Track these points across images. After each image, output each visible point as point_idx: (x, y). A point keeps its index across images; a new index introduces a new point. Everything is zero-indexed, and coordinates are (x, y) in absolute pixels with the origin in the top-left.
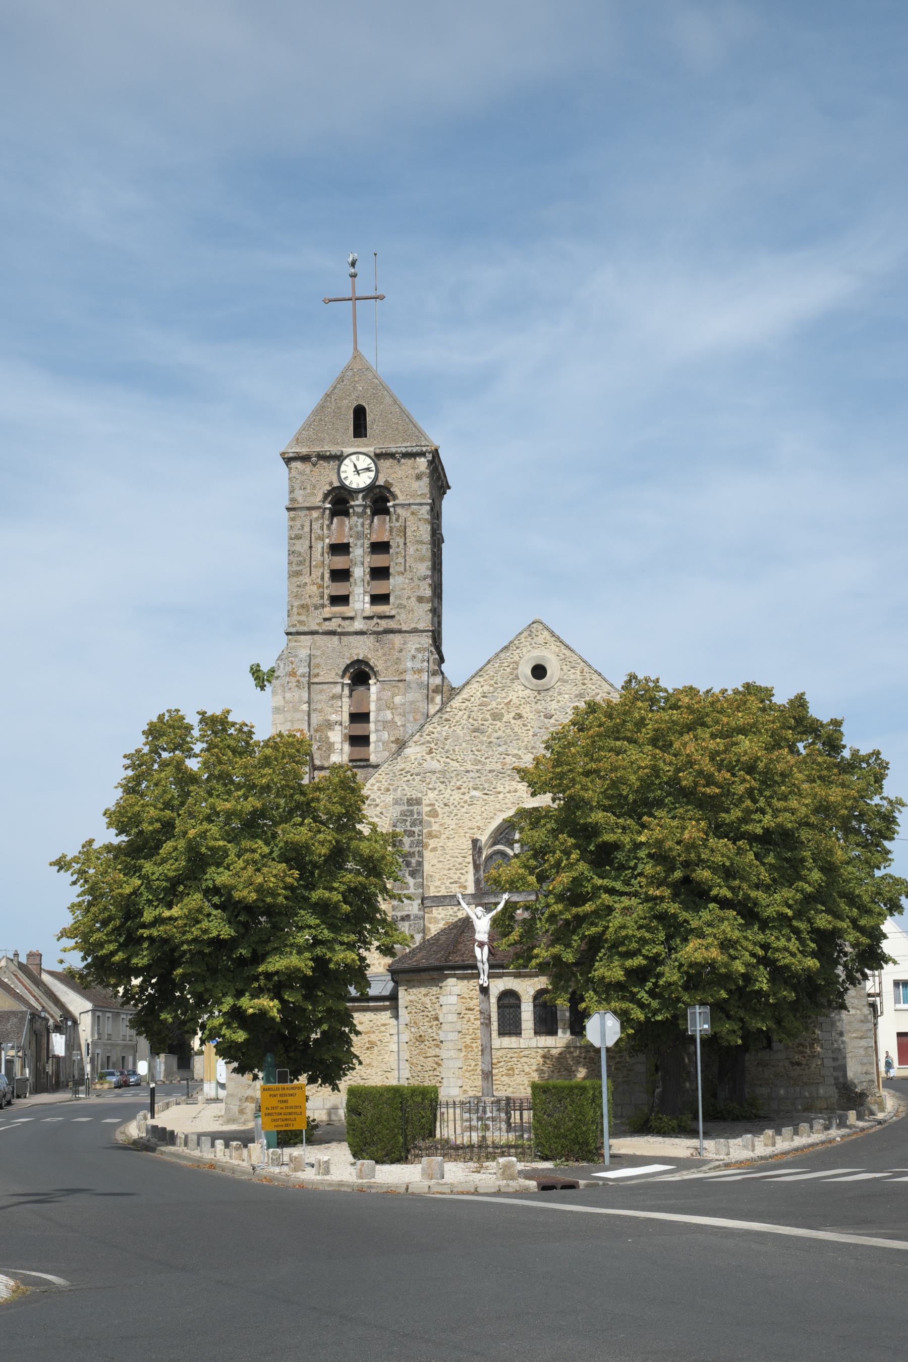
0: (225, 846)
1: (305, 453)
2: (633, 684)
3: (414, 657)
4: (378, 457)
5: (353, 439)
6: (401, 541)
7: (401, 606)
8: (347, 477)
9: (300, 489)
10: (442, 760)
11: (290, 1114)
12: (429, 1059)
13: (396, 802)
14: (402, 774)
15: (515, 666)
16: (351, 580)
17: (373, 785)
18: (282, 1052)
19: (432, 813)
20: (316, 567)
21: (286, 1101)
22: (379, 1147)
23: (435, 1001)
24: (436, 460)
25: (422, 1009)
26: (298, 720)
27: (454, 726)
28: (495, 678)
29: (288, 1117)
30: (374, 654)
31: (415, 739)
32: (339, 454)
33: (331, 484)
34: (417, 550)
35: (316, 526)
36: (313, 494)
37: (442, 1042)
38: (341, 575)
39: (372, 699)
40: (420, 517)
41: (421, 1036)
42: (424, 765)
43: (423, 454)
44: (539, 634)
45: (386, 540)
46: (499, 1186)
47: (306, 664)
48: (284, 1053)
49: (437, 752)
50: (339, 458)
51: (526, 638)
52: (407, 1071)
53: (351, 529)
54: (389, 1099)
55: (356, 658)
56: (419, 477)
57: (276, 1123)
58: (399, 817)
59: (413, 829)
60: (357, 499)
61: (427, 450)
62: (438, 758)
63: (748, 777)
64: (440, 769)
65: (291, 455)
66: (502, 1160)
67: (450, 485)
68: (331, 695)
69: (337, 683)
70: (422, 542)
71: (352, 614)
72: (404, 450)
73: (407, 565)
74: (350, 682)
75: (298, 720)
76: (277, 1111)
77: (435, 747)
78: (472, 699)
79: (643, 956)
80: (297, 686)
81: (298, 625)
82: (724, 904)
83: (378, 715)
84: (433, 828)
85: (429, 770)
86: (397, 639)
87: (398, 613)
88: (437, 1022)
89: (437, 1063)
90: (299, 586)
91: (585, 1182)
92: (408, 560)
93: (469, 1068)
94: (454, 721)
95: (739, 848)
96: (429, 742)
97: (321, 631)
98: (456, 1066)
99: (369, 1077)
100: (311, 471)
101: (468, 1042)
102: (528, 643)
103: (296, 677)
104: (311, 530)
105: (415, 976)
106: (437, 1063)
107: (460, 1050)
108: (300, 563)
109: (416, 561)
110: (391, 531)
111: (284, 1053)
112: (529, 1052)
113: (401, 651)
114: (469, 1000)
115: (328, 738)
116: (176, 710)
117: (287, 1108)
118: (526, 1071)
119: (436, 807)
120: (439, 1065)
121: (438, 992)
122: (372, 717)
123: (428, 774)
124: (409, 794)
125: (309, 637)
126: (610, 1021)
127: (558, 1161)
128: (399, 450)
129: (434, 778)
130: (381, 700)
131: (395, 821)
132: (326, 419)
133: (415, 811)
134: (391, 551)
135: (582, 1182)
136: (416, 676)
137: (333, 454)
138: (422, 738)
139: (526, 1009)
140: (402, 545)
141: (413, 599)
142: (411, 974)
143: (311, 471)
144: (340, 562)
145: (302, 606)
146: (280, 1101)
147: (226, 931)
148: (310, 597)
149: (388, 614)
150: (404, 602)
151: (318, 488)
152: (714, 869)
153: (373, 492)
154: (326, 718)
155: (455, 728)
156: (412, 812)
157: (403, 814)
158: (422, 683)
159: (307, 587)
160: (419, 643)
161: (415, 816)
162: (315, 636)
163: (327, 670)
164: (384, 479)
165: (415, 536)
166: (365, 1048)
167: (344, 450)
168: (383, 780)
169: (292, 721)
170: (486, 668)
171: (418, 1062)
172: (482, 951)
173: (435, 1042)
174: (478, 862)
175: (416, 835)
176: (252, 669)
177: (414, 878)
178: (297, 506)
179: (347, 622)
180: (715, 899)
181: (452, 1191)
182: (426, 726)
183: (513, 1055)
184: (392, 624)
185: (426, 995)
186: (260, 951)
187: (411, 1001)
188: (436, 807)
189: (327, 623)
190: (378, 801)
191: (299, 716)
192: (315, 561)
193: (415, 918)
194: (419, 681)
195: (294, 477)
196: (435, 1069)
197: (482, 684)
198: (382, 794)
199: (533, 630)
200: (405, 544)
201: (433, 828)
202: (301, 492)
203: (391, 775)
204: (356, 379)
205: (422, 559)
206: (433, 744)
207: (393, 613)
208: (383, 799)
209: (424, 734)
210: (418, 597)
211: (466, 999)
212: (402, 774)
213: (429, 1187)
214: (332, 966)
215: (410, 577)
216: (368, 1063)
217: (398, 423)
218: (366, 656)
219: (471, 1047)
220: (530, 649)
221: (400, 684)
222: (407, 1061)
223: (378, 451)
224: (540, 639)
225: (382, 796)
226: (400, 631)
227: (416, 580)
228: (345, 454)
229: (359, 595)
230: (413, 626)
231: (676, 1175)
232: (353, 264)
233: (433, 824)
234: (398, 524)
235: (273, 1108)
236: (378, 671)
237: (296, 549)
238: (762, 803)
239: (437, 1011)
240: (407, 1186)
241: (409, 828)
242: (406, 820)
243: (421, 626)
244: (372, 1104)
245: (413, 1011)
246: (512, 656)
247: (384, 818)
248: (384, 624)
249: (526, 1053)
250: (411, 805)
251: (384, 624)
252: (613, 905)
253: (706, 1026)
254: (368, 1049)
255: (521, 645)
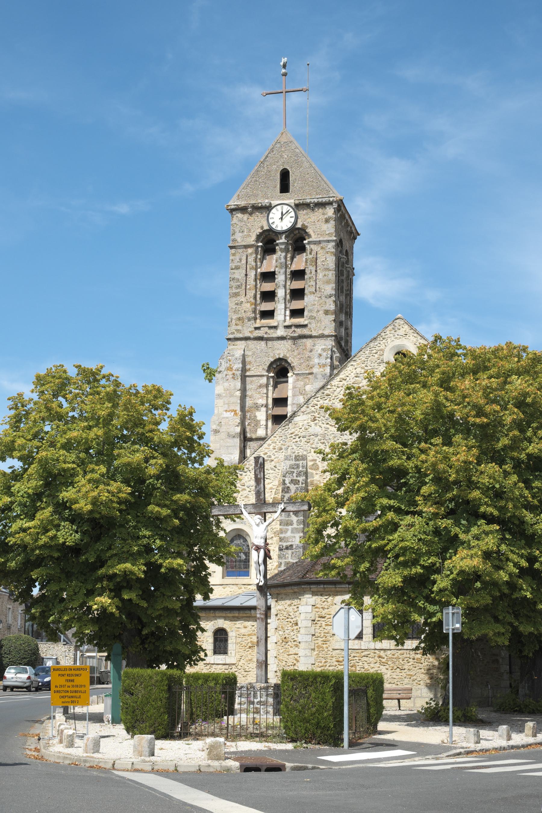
0: (73, 469)
1: (243, 205)
2: (438, 343)
3: (320, 355)
4: (298, 206)
5: (279, 194)
6: (313, 269)
7: (312, 318)
8: (274, 222)
9: (240, 232)
10: (323, 426)
11: (76, 692)
12: (291, 656)
13: (287, 458)
14: (292, 437)
15: (382, 353)
16: (276, 299)
17: (269, 445)
18: (138, 643)
19: (314, 466)
20: (250, 289)
21: (72, 681)
22: (147, 724)
23: (296, 610)
24: (342, 208)
25: (287, 616)
26: (233, 403)
27: (334, 399)
28: (366, 362)
29: (74, 694)
30: (291, 353)
31: (302, 410)
32: (268, 205)
33: (262, 227)
34: (325, 275)
35: (251, 259)
36: (250, 236)
37: (300, 643)
38: (269, 296)
39: (289, 388)
40: (327, 250)
41: (285, 638)
42: (309, 430)
43: (330, 203)
44: (400, 327)
45: (302, 268)
46: (199, 766)
47: (240, 361)
48: (140, 644)
49: (319, 419)
50: (268, 208)
51: (390, 331)
52: (275, 665)
53: (276, 261)
54: (157, 681)
55: (277, 357)
56: (327, 221)
57: (63, 700)
58: (288, 470)
59: (298, 478)
60: (281, 239)
61: (333, 200)
62: (320, 424)
63: (516, 410)
64: (321, 433)
65: (233, 207)
66: (210, 740)
67: (359, 232)
68: (259, 384)
69: (263, 376)
70: (328, 269)
71: (275, 324)
72: (316, 200)
73: (317, 286)
74: (273, 375)
75: (233, 403)
76: (65, 689)
77: (318, 416)
78: (348, 378)
79: (420, 565)
80: (233, 378)
81: (236, 333)
82: (490, 520)
83: (293, 399)
84: (314, 479)
85: (313, 433)
86: (309, 342)
87: (310, 323)
88: (297, 627)
89: (296, 660)
90: (237, 304)
91: (292, 765)
92: (318, 283)
93: (321, 664)
94: (333, 396)
95: (505, 471)
96: (313, 412)
97: (252, 337)
98: (309, 662)
99: (250, 669)
100: (248, 219)
101: (320, 643)
102: (392, 335)
103: (232, 371)
104: (247, 262)
105: (282, 590)
106: (296, 660)
107: (313, 650)
108: (239, 287)
109: (323, 284)
110: (306, 262)
111: (140, 644)
112: (369, 653)
113: (311, 351)
114: (321, 610)
115: (256, 416)
116: (60, 366)
117: (73, 686)
118: (366, 668)
119: (317, 462)
120: (298, 661)
121: (299, 603)
122: (289, 402)
123: (312, 437)
124: (297, 452)
125: (243, 342)
126: (353, 616)
127: (298, 743)
128: (312, 201)
129: (317, 439)
130: (296, 388)
131: (285, 473)
132: (260, 180)
133: (301, 465)
134: (306, 277)
135: (288, 765)
136: (321, 370)
137: (264, 205)
138: (308, 409)
139: (367, 618)
140: (313, 272)
141: (321, 312)
142: (279, 589)
143: (248, 219)
144: (267, 287)
145: (239, 319)
146: (67, 681)
147: (71, 539)
148: (245, 312)
149: (302, 323)
150: (314, 314)
151: (252, 231)
152: (486, 490)
153: (293, 233)
154: (255, 402)
155: (334, 401)
156: (298, 466)
157: (291, 467)
158: (325, 374)
159: (243, 305)
160: (325, 345)
161: (301, 469)
162: (249, 342)
163: (256, 366)
164: (302, 223)
165: (323, 265)
166: (248, 647)
167: (272, 202)
168: (278, 442)
169: (228, 404)
170: (359, 355)
171: (284, 659)
172: (259, 553)
173: (295, 643)
174: (259, 476)
175: (300, 483)
176: (203, 366)
177: (297, 516)
178: (237, 244)
179: (272, 331)
180: (484, 516)
181: (153, 769)
182: (312, 400)
183: (355, 655)
184: (305, 331)
185: (290, 605)
186: (104, 558)
187: (280, 610)
188: (317, 462)
189: (257, 331)
190: (273, 457)
191: (233, 400)
192: (249, 285)
193: (296, 547)
194: (323, 373)
195: (235, 224)
196: (295, 664)
197: (356, 367)
198: (276, 452)
199: (396, 325)
200: (316, 271)
201: (314, 479)
202: (240, 234)
203: (284, 437)
204: (283, 149)
205: (328, 282)
206: (316, 414)
207: (306, 323)
208: (277, 456)
209: (310, 406)
210: (325, 310)
211: (319, 608)
212: (292, 437)
213: (133, 764)
214: (163, 570)
215: (319, 296)
216: (250, 658)
217: (313, 181)
218: (285, 356)
219: (322, 647)
220: (393, 339)
221: (310, 376)
222: (276, 657)
223: (297, 202)
224: (401, 332)
225: (276, 453)
226: (310, 337)
227: (323, 298)
228: (273, 206)
229: (281, 309)
230: (320, 332)
231: (417, 759)
232: (284, 66)
233: (315, 475)
234: (310, 256)
235: (61, 686)
236: (294, 366)
237: (236, 277)
238: (529, 433)
239: (297, 618)
240: (114, 761)
241: (295, 478)
242: (294, 472)
243: (326, 332)
244: (143, 686)
245: (281, 618)
246: (379, 345)
247: (277, 470)
248: (299, 331)
249: (366, 653)
250: (298, 460)
251: (299, 331)
252: (399, 522)
253: (458, 626)
254: (250, 647)
255: (386, 337)
